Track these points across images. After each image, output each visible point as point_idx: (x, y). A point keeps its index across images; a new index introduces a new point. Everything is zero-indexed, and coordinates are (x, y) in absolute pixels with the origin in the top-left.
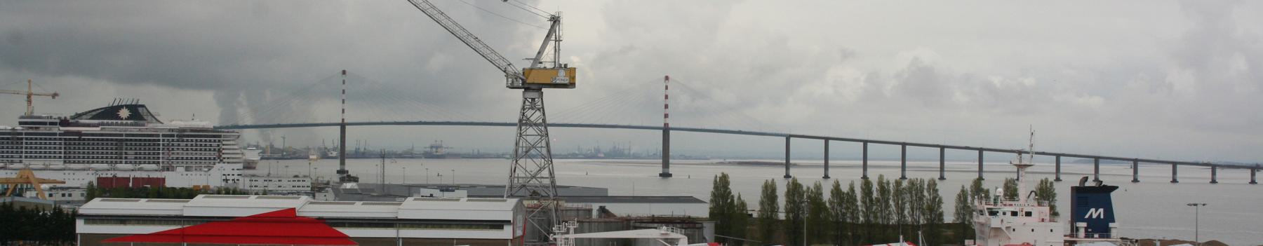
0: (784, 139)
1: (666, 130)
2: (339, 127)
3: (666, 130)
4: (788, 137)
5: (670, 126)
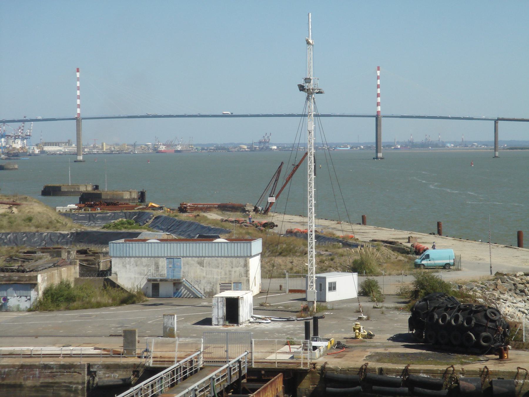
0: (493, 122)
2: (375, 118)
3: (377, 117)
4: (496, 121)
5: (382, 114)
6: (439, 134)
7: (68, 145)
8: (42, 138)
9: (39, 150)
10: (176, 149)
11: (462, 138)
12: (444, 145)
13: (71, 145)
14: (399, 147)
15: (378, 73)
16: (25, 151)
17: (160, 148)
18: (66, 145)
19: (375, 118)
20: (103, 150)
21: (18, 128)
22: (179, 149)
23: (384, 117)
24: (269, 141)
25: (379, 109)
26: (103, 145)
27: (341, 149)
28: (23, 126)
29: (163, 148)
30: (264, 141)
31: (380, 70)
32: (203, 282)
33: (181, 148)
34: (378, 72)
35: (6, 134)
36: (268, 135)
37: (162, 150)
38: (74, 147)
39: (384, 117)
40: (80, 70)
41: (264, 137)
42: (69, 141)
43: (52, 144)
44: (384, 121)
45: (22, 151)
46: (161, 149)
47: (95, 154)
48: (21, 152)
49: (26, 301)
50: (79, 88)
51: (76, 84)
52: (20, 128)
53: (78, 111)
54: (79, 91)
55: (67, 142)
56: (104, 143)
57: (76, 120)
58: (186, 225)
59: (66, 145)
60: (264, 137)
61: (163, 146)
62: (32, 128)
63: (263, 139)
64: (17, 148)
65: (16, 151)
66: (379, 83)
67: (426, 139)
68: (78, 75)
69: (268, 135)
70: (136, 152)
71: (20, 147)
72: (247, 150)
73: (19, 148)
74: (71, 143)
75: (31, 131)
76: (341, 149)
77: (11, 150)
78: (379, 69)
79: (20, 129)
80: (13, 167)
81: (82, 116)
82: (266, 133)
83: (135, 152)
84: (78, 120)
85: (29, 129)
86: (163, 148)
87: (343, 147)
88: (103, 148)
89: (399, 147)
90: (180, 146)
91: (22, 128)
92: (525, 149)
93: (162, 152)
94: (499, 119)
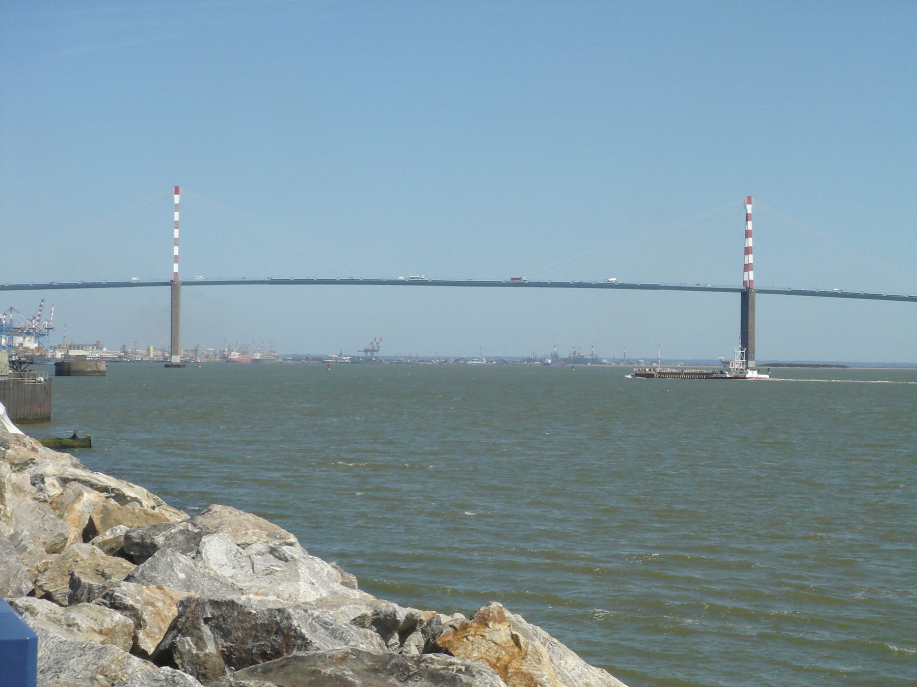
1: (746, 296)
3: (746, 296)
5: (756, 286)
6: (592, 347)
7: (97, 349)
8: (65, 334)
9: (63, 353)
10: (253, 357)
11: (625, 353)
13: (101, 348)
14: (550, 362)
15: (749, 208)
16: (43, 354)
17: (232, 355)
18: (93, 348)
19: (740, 294)
20: (150, 356)
21: (31, 318)
22: (257, 358)
23: (760, 291)
24: (378, 349)
25: (751, 275)
26: (149, 350)
27: (473, 362)
28: (39, 315)
29: (235, 355)
30: (373, 349)
31: (753, 203)
32: (60, 459)
33: (261, 356)
35: (14, 327)
36: (378, 340)
37: (234, 359)
38: (105, 352)
39: (760, 291)
41: (372, 343)
42: (98, 342)
43: (80, 347)
44: (760, 302)
45: (39, 354)
46: (233, 358)
47: (138, 361)
48: (37, 354)
50: (178, 225)
52: (34, 318)
53: (176, 268)
54: (177, 230)
55: (95, 345)
56: (152, 347)
57: (170, 287)
58: (401, 492)
59: (93, 348)
60: (372, 343)
61: (235, 353)
62: (51, 319)
63: (370, 346)
64: (31, 348)
67: (575, 353)
68: (177, 199)
69: (378, 340)
70: (199, 361)
71: (36, 348)
72: (347, 361)
73: (34, 348)
74: (100, 346)
75: (51, 323)
76: (473, 362)
77: (22, 352)
79: (34, 319)
80: (95, 369)
82: (375, 339)
83: (196, 361)
84: (174, 285)
85: (47, 321)
86: (235, 355)
87: (476, 361)
88: (149, 354)
89: (550, 362)
90: (259, 353)
91: (38, 318)
92: (780, 366)
93: (234, 362)
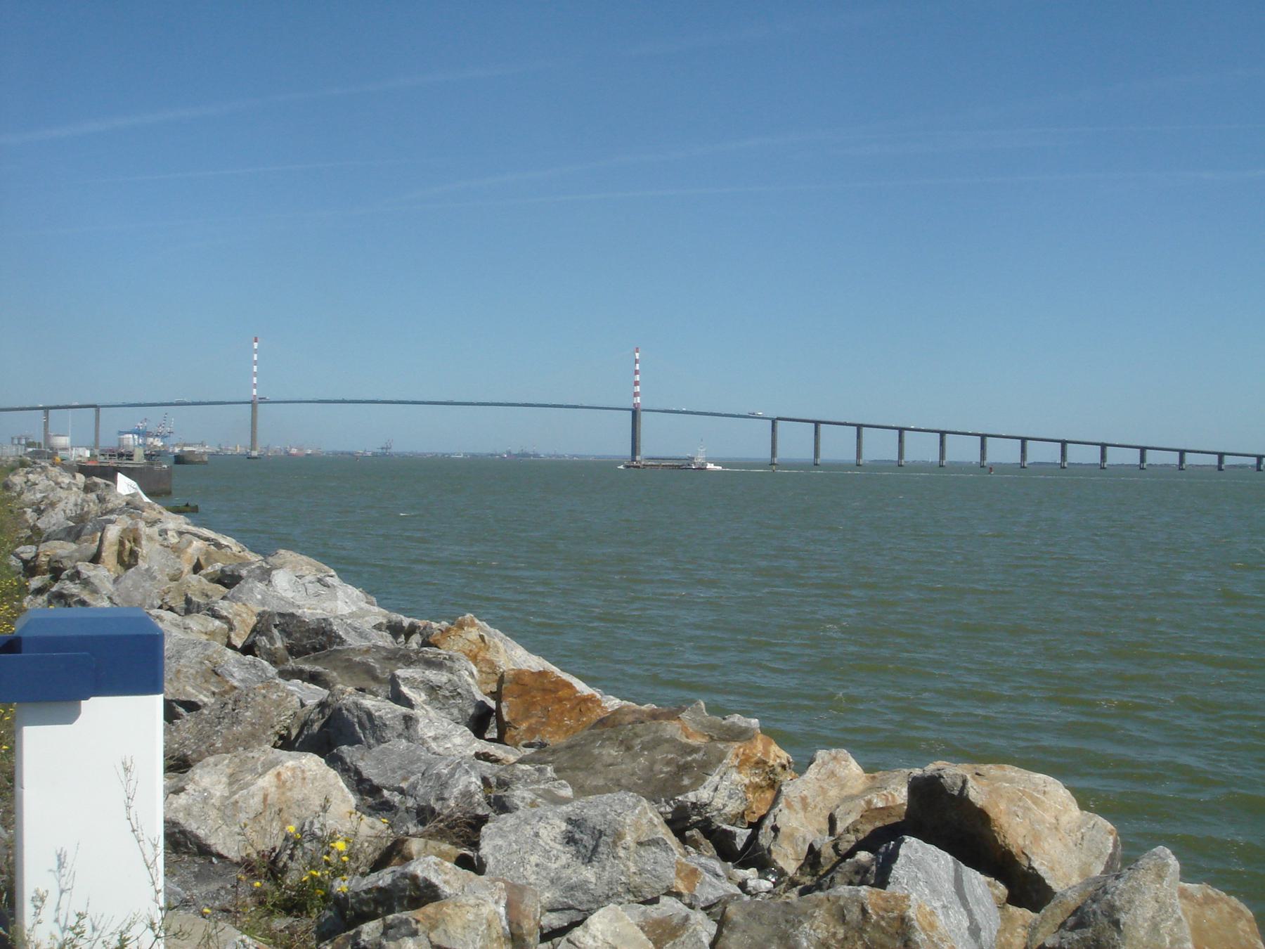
0: (770, 422)
2: (630, 412)
3: (635, 413)
4: (774, 422)
12: (564, 456)
23: (644, 410)
25: (638, 400)
29: (294, 451)
34: (637, 354)
39: (644, 410)
40: (259, 340)
44: (644, 418)
49: (832, 821)
51: (258, 356)
53: (255, 392)
65: (158, 449)
66: (638, 368)
68: (256, 345)
78: (256, 341)
81: (642, 407)
94: (779, 419)
